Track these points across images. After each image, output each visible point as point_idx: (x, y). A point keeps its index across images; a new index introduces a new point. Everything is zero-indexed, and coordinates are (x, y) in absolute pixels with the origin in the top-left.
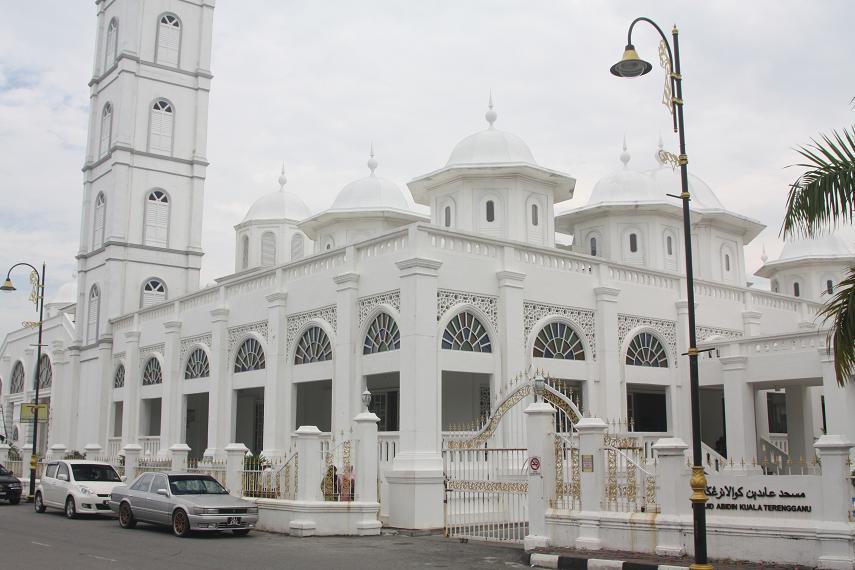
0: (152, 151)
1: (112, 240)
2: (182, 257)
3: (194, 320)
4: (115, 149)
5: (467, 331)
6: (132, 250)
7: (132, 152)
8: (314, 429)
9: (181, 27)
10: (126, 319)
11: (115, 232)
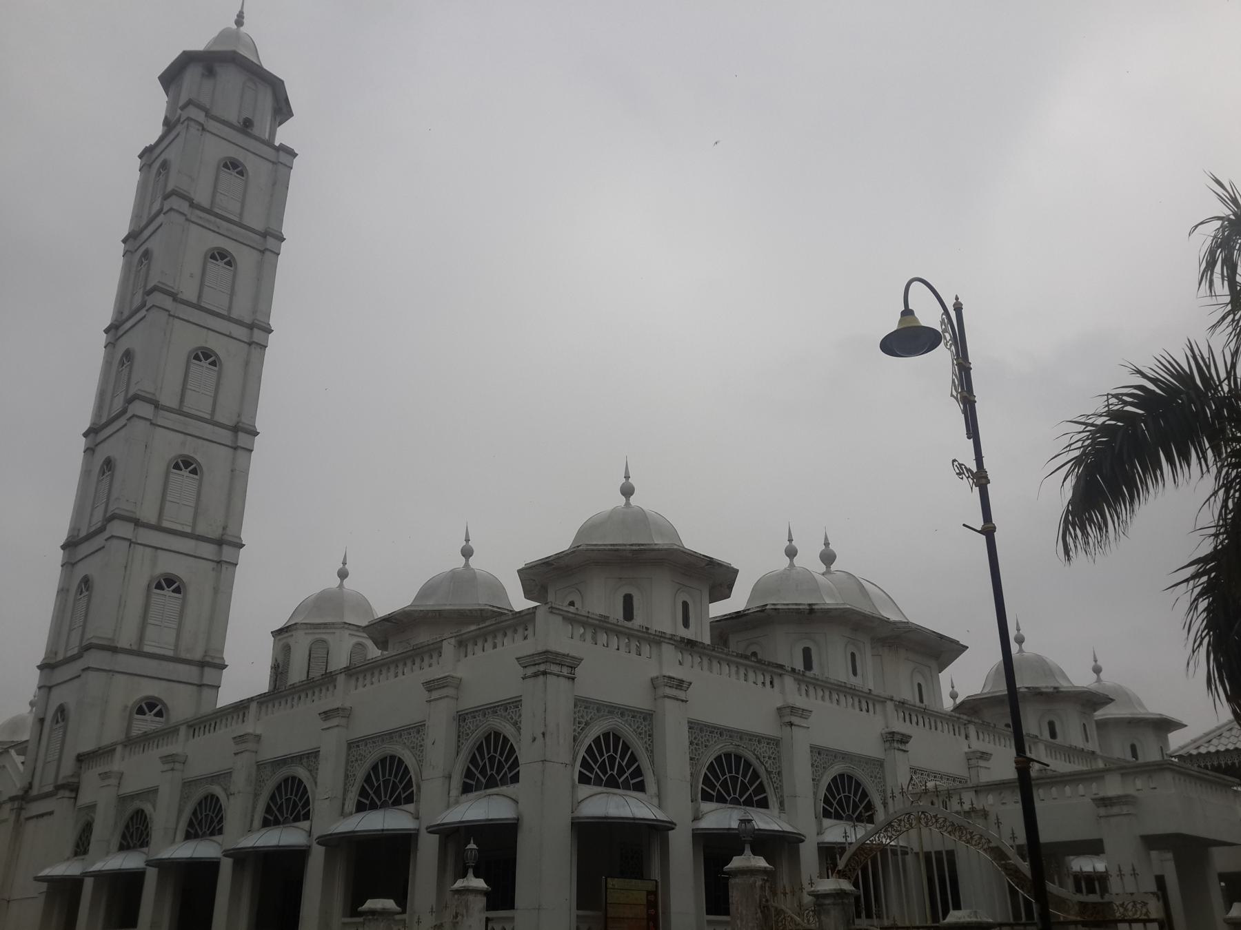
0: (165, 524)
1: (95, 641)
2: (195, 670)
3: (207, 754)
4: (113, 517)
5: (612, 761)
6: (122, 658)
7: (137, 523)
8: (390, 904)
9: (220, 369)
10: (101, 754)
11: (100, 628)
